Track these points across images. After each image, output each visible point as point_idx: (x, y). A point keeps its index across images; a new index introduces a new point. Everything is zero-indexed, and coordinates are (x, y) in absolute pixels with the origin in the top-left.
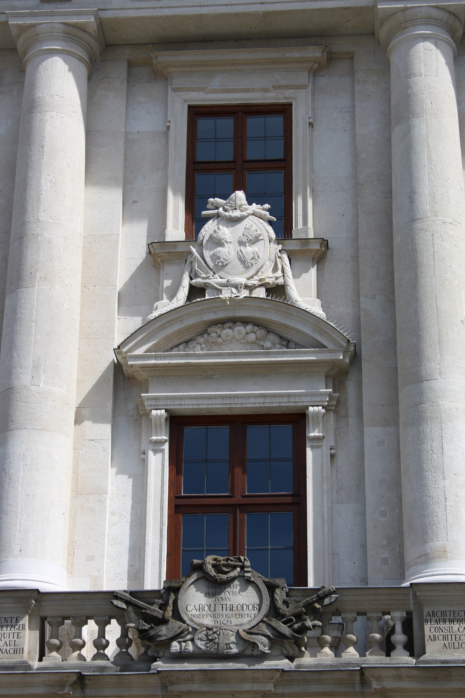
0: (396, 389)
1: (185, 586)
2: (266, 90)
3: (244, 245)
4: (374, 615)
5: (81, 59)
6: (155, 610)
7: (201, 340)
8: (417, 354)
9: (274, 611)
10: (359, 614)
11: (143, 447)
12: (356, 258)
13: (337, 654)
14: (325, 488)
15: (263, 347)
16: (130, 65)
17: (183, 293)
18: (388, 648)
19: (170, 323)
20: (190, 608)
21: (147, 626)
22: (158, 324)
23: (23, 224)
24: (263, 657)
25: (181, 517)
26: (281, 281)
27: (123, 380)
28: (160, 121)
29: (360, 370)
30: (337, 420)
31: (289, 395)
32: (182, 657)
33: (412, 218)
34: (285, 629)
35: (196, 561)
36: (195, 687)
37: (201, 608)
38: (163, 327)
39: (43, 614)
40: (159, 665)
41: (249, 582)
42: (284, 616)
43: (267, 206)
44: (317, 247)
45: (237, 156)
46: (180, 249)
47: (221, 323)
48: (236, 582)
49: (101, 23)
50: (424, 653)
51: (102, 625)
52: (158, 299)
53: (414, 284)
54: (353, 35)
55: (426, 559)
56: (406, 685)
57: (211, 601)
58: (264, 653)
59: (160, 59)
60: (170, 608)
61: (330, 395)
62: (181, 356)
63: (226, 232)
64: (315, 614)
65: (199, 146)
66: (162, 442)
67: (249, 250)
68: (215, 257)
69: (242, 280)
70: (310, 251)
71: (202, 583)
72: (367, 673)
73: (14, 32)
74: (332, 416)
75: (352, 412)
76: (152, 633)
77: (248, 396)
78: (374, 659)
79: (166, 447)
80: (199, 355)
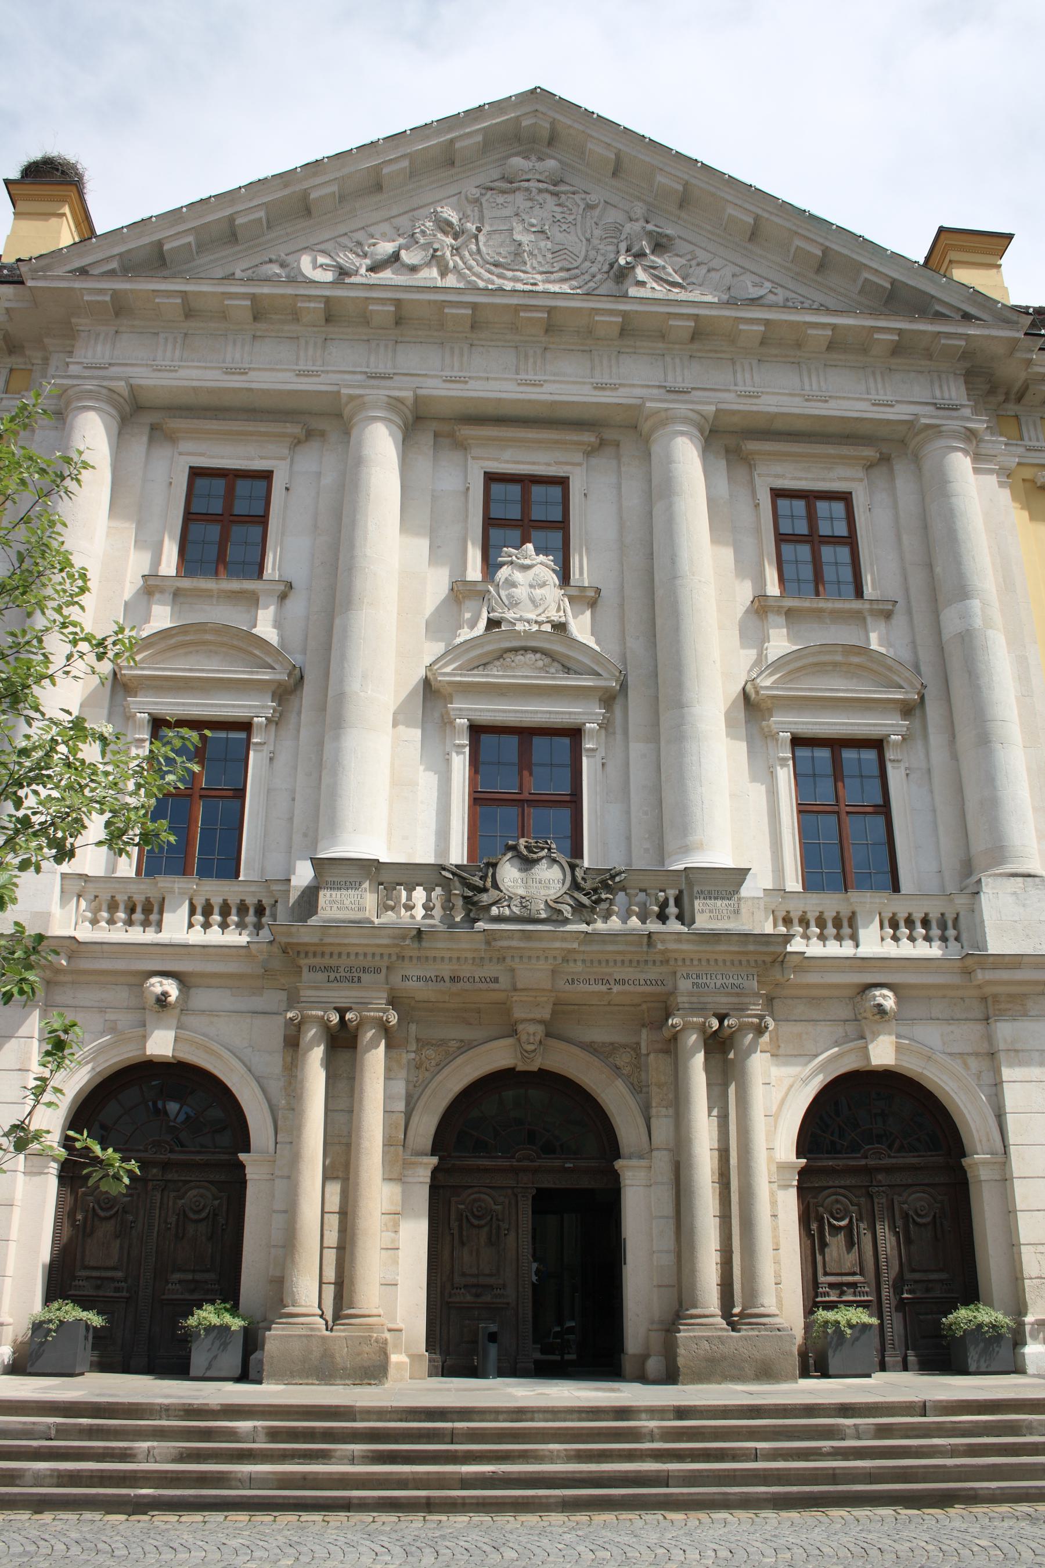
0: (656, 713)
1: (502, 862)
2: (548, 464)
3: (531, 587)
4: (653, 892)
5: (399, 427)
6: (477, 881)
7: (497, 663)
8: (678, 685)
9: (575, 886)
10: (641, 890)
11: (447, 750)
12: (622, 606)
13: (624, 922)
14: (598, 789)
15: (547, 672)
16: (436, 435)
17: (482, 624)
18: (662, 917)
19: (473, 647)
20: (506, 880)
21: (471, 894)
22: (464, 648)
23: (352, 557)
24: (566, 921)
25: (478, 807)
26: (563, 620)
27: (431, 692)
28: (461, 481)
29: (627, 695)
30: (606, 736)
31: (570, 713)
32: (499, 919)
33: (674, 576)
34: (585, 900)
35: (510, 842)
36: (514, 943)
37: (515, 881)
38: (467, 651)
39: (381, 880)
40: (480, 925)
41: (555, 861)
42: (584, 890)
43: (551, 558)
44: (593, 594)
45: (524, 514)
46: (480, 587)
47: (515, 650)
48: (544, 861)
49: (417, 398)
50: (694, 922)
51: (429, 890)
52: (460, 627)
53: (676, 629)
54: (620, 427)
55: (686, 850)
56: (685, 947)
57: (524, 875)
58: (567, 919)
59: (462, 432)
60: (489, 880)
61: (603, 715)
62: (483, 676)
63: (518, 576)
64: (608, 888)
65: (492, 506)
66: (463, 746)
67: (538, 592)
68: (510, 596)
69: (532, 616)
70: (586, 597)
71: (516, 861)
72: (654, 937)
73: (344, 400)
74: (603, 731)
75: (619, 730)
76: (476, 899)
77: (537, 712)
78: (654, 926)
79: (467, 749)
80: (496, 676)
